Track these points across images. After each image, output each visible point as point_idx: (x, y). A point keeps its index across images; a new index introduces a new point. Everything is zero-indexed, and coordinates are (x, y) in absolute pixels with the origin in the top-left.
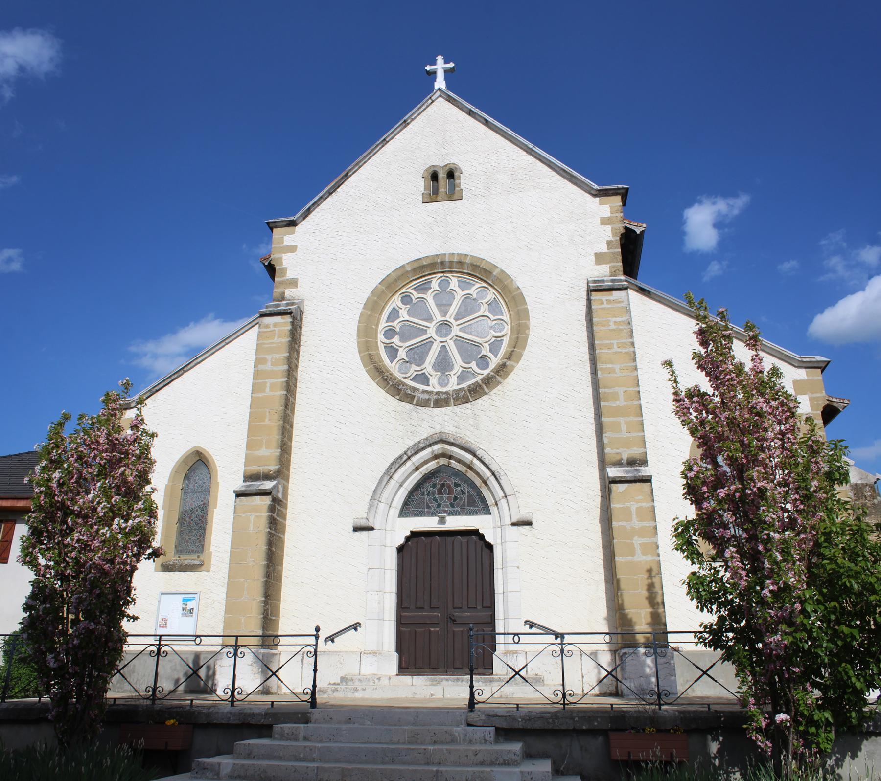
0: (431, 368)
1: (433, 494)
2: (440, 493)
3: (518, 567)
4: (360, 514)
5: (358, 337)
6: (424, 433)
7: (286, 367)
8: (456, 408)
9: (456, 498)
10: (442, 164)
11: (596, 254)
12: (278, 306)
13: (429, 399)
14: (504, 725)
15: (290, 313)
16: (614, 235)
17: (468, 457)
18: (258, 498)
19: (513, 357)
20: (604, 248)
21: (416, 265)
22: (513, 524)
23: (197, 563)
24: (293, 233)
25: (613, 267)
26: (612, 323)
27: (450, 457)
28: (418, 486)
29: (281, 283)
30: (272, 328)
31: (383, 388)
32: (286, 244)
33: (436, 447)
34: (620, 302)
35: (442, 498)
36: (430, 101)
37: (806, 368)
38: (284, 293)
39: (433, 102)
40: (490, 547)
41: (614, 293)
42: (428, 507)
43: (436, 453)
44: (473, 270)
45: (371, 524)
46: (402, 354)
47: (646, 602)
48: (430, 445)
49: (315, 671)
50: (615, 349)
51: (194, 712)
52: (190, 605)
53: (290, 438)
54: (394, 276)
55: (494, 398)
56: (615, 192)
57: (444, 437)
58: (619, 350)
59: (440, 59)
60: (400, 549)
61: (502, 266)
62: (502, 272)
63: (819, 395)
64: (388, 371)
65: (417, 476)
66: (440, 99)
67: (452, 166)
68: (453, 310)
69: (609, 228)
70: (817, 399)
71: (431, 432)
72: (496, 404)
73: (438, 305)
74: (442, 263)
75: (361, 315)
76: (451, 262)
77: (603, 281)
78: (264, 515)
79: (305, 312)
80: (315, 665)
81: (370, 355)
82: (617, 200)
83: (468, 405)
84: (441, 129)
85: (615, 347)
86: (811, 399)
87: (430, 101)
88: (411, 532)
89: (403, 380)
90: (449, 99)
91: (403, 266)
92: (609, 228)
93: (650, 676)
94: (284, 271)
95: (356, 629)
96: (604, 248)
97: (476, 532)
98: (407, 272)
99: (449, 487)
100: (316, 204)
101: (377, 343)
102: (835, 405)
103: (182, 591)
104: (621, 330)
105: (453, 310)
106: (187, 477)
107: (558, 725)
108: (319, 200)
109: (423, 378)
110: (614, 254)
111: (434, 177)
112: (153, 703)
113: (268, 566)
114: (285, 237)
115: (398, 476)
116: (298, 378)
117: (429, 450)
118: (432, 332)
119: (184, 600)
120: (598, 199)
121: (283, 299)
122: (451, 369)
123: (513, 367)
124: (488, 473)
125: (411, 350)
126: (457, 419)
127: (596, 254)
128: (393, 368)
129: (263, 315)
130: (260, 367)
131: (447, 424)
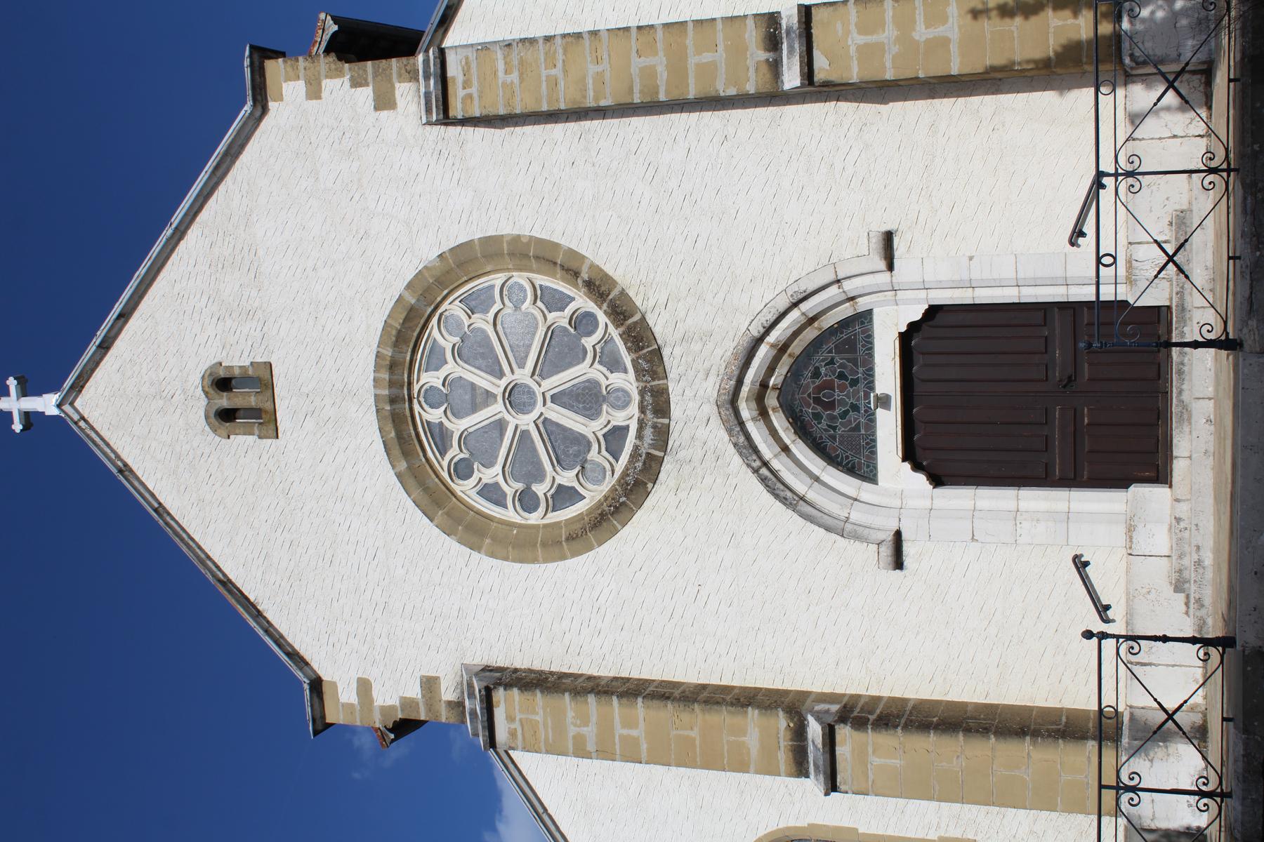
1: (832, 418)
3: (971, 258)
4: (869, 557)
6: (718, 436)
8: (672, 375)
9: (842, 376)
11: (376, 108)
13: (654, 427)
16: (340, 74)
17: (763, 351)
18: (839, 750)
19: (574, 265)
20: (365, 94)
21: (396, 451)
22: (890, 267)
24: (334, 685)
26: (509, 78)
27: (764, 386)
28: (818, 448)
30: (517, 725)
31: (633, 513)
34: (467, 58)
35: (842, 402)
36: (82, 424)
38: (449, 703)
39: (83, 418)
40: (933, 312)
42: (857, 428)
43: (755, 413)
44: (406, 342)
45: (889, 536)
48: (741, 424)
49: (1165, 639)
53: (727, 689)
54: (417, 493)
55: (651, 303)
58: (560, 65)
60: (937, 480)
61: (398, 287)
62: (409, 286)
64: (600, 504)
65: (800, 450)
66: (77, 404)
67: (208, 382)
68: (483, 381)
69: (328, 85)
71: (716, 422)
72: (663, 300)
76: (391, 384)
77: (427, 95)
78: (871, 738)
79: (485, 662)
81: (570, 538)
82: (274, 68)
83: (666, 353)
84: (135, 400)
85: (553, 72)
88: (904, 460)
89: (617, 475)
90: (78, 387)
91: (399, 476)
92: (328, 85)
94: (407, 703)
95: (1086, 564)
96: (365, 94)
97: (905, 338)
98: (409, 468)
99: (819, 389)
100: (280, 640)
101: (545, 526)
104: (521, 62)
105: (483, 381)
109: (615, 437)
110: (375, 75)
111: (227, 416)
114: (343, 698)
117: (751, 426)
118: (526, 421)
120: (271, 105)
121: (459, 705)
123: (593, 267)
124: (795, 315)
125: (560, 461)
126: (691, 373)
127: (376, 108)
128: (593, 494)
129: (492, 742)
130: (591, 747)
131: (701, 393)
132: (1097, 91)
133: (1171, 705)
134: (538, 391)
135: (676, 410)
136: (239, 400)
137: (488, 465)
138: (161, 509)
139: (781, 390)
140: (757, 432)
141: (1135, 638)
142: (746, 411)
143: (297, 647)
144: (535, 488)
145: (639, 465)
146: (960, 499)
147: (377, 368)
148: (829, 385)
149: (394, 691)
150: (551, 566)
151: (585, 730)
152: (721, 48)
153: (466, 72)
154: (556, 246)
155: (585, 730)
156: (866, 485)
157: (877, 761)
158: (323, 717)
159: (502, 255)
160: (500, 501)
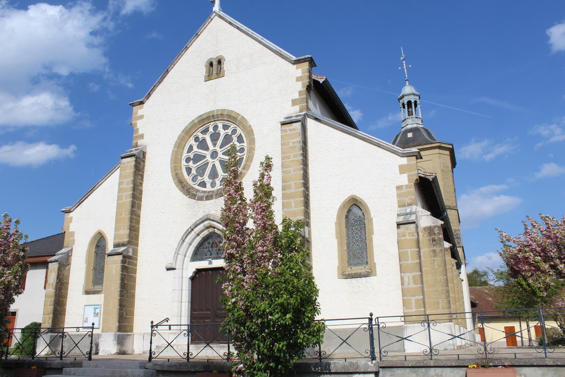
0: (207, 177)
1: (209, 248)
2: (212, 247)
4: (169, 261)
5: (171, 164)
6: (201, 215)
7: (132, 185)
9: (219, 250)
10: (215, 57)
11: (292, 100)
12: (131, 151)
13: (203, 196)
14: (159, 369)
16: (303, 87)
18: (117, 256)
19: (246, 168)
20: (296, 96)
21: (200, 119)
23: (100, 290)
24: (142, 108)
25: (301, 106)
26: (291, 143)
27: (214, 228)
28: (201, 244)
29: (136, 137)
30: (126, 165)
31: (182, 192)
32: (139, 114)
33: (206, 223)
34: (296, 130)
35: (213, 250)
36: (210, 20)
38: (137, 143)
39: (212, 19)
41: (294, 124)
42: (206, 255)
44: (229, 118)
45: (174, 267)
46: (194, 172)
48: (203, 222)
49: (151, 343)
50: (292, 158)
51: (47, 363)
52: (98, 311)
53: (138, 222)
54: (189, 127)
56: (304, 60)
57: (209, 217)
58: (294, 159)
60: (193, 279)
61: (242, 114)
62: (243, 117)
63: (413, 173)
64: (186, 181)
65: (199, 239)
66: (216, 17)
67: (220, 57)
68: (219, 142)
69: (300, 83)
70: (412, 175)
73: (212, 141)
74: (213, 116)
75: (173, 151)
76: (217, 115)
77: (291, 117)
78: (119, 265)
79: (147, 152)
80: (151, 341)
81: (176, 174)
82: (306, 65)
84: (220, 35)
85: (292, 157)
86: (409, 176)
87: (210, 20)
89: (194, 186)
90: (220, 17)
91: (193, 121)
92: (300, 83)
94: (137, 130)
96: (296, 96)
98: (195, 124)
99: (216, 243)
100: (153, 90)
101: (181, 166)
102: (428, 177)
103: (94, 304)
104: (295, 147)
105: (219, 142)
107: (182, 369)
108: (154, 87)
109: (203, 184)
110: (302, 99)
111: (211, 64)
113: (121, 291)
114: (139, 111)
115: (188, 240)
116: (143, 190)
117: (202, 224)
118: (208, 158)
119: (95, 309)
120: (295, 66)
121: (137, 146)
122: (217, 177)
123: (245, 173)
125: (198, 169)
127: (292, 100)
128: (188, 179)
129: (123, 158)
130: (121, 186)
132: (520, 323)
133: (208, 348)
134: (215, 160)
135: (207, 202)
136: (215, 68)
137: (198, 147)
138: (187, 48)
139: (214, 233)
140: (201, 227)
141: (92, 336)
142: (206, 223)
143: (152, 95)
144: (192, 161)
145: (194, 193)
146: (186, 286)
147: (221, 110)
148: (217, 246)
149: (141, 126)
150: (170, 169)
151: (125, 184)
152: (295, 209)
153: (294, 130)
154: (251, 162)
155: (125, 184)
156: (190, 259)
157: (114, 267)
158: (135, 106)
159: (250, 145)
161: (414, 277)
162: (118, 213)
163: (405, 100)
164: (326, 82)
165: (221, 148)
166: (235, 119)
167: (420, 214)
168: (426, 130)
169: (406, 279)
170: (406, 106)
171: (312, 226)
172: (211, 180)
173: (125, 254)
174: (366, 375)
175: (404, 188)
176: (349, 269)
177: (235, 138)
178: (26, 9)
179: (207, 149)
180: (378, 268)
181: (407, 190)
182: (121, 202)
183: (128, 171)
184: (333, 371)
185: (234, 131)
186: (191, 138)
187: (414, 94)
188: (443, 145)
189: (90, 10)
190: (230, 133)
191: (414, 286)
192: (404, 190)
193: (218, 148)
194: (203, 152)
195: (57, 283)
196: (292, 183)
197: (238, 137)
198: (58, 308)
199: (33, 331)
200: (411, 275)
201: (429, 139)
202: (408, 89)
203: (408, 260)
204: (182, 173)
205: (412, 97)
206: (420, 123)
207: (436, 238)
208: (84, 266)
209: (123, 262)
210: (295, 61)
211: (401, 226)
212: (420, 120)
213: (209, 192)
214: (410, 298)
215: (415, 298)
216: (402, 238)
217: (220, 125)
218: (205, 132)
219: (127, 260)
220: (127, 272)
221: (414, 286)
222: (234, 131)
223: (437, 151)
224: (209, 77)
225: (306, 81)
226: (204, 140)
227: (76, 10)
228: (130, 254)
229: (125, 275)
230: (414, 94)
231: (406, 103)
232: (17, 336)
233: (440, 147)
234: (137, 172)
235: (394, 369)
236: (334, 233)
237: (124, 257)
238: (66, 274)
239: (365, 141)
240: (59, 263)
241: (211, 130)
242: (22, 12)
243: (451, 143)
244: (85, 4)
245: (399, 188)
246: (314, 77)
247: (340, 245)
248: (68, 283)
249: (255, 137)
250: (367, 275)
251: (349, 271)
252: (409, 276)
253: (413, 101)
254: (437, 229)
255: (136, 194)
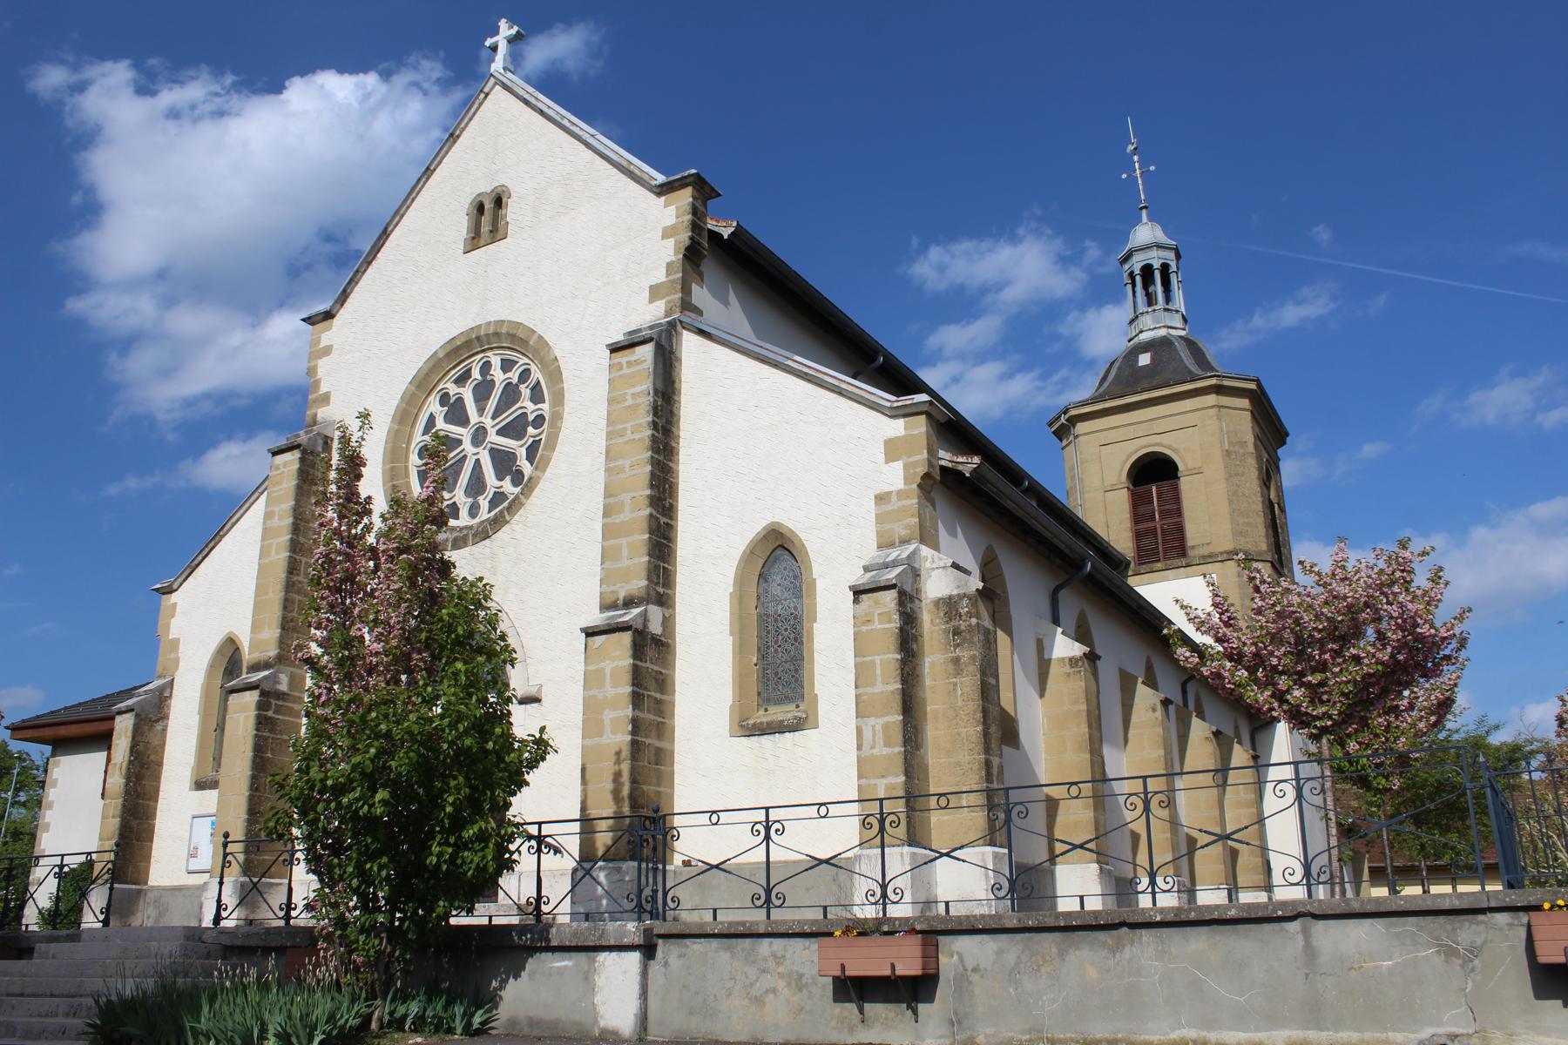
7: (291, 520)
15: (298, 446)
16: (676, 253)
21: (450, 348)
24: (330, 328)
37: (905, 416)
47: (610, 797)
50: (629, 436)
54: (426, 369)
59: (503, 24)
61: (540, 330)
62: (541, 337)
70: (914, 465)
73: (476, 401)
74: (478, 338)
82: (686, 196)
86: (906, 467)
93: (601, 897)
101: (406, 468)
102: (960, 468)
104: (638, 405)
106: (762, 576)
110: (672, 282)
111: (480, 208)
112: (288, 922)
113: (253, 777)
118: (467, 446)
121: (315, 423)
123: (539, 478)
136: (488, 217)
152: (629, 562)
160: (426, 431)
161: (885, 727)
162: (260, 590)
163: (1137, 263)
164: (739, 233)
165: (494, 418)
166: (524, 342)
167: (928, 565)
168: (1190, 343)
169: (867, 734)
170: (1138, 279)
171: (678, 607)
172: (470, 500)
173: (266, 687)
174: (623, 954)
175: (894, 498)
176: (762, 712)
177: (525, 391)
178: (277, 88)
179: (463, 420)
180: (823, 708)
181: (900, 504)
182: (266, 561)
183: (284, 485)
184: (554, 943)
185: (525, 375)
186: (431, 398)
187: (1159, 246)
188: (1226, 383)
189: (438, 81)
190: (515, 380)
191: (886, 751)
192: (895, 504)
193: (488, 422)
194: (455, 430)
195: (130, 762)
196: (626, 498)
197: (533, 389)
198: (134, 823)
199: (75, 881)
200: (880, 722)
201: (1194, 368)
202: (1146, 232)
203: (873, 684)
204: (408, 484)
205: (1154, 253)
206: (1179, 324)
207: (963, 625)
208: (195, 720)
209: (262, 706)
210: (661, 186)
211: (864, 597)
212: (1178, 316)
213: (462, 529)
214: (873, 781)
215: (885, 781)
216: (864, 628)
217: (496, 361)
218: (462, 380)
219: (274, 702)
220: (271, 731)
221: (886, 751)
222: (525, 375)
223: (1211, 399)
224: (475, 240)
225: (685, 236)
226: (460, 400)
227: (402, 79)
228: (284, 687)
229: (266, 739)
230: (1159, 246)
231: (1137, 271)
232: (44, 892)
233: (1219, 390)
234: (306, 487)
235: (687, 941)
236: (727, 621)
237: (263, 694)
238: (155, 742)
239: (809, 381)
240: (137, 715)
241: (476, 374)
242: (272, 98)
243: (1252, 375)
244: (426, 65)
245: (881, 499)
246: (711, 224)
247: (740, 649)
248: (160, 764)
249: (565, 386)
250: (796, 726)
251: (761, 717)
252: (875, 724)
253: (1156, 264)
254: (965, 602)
255: (302, 540)
